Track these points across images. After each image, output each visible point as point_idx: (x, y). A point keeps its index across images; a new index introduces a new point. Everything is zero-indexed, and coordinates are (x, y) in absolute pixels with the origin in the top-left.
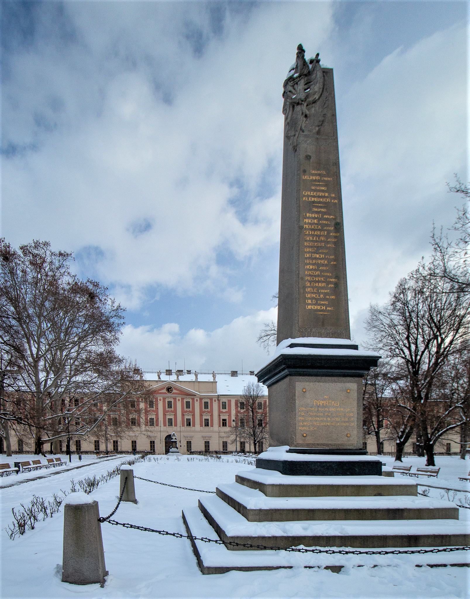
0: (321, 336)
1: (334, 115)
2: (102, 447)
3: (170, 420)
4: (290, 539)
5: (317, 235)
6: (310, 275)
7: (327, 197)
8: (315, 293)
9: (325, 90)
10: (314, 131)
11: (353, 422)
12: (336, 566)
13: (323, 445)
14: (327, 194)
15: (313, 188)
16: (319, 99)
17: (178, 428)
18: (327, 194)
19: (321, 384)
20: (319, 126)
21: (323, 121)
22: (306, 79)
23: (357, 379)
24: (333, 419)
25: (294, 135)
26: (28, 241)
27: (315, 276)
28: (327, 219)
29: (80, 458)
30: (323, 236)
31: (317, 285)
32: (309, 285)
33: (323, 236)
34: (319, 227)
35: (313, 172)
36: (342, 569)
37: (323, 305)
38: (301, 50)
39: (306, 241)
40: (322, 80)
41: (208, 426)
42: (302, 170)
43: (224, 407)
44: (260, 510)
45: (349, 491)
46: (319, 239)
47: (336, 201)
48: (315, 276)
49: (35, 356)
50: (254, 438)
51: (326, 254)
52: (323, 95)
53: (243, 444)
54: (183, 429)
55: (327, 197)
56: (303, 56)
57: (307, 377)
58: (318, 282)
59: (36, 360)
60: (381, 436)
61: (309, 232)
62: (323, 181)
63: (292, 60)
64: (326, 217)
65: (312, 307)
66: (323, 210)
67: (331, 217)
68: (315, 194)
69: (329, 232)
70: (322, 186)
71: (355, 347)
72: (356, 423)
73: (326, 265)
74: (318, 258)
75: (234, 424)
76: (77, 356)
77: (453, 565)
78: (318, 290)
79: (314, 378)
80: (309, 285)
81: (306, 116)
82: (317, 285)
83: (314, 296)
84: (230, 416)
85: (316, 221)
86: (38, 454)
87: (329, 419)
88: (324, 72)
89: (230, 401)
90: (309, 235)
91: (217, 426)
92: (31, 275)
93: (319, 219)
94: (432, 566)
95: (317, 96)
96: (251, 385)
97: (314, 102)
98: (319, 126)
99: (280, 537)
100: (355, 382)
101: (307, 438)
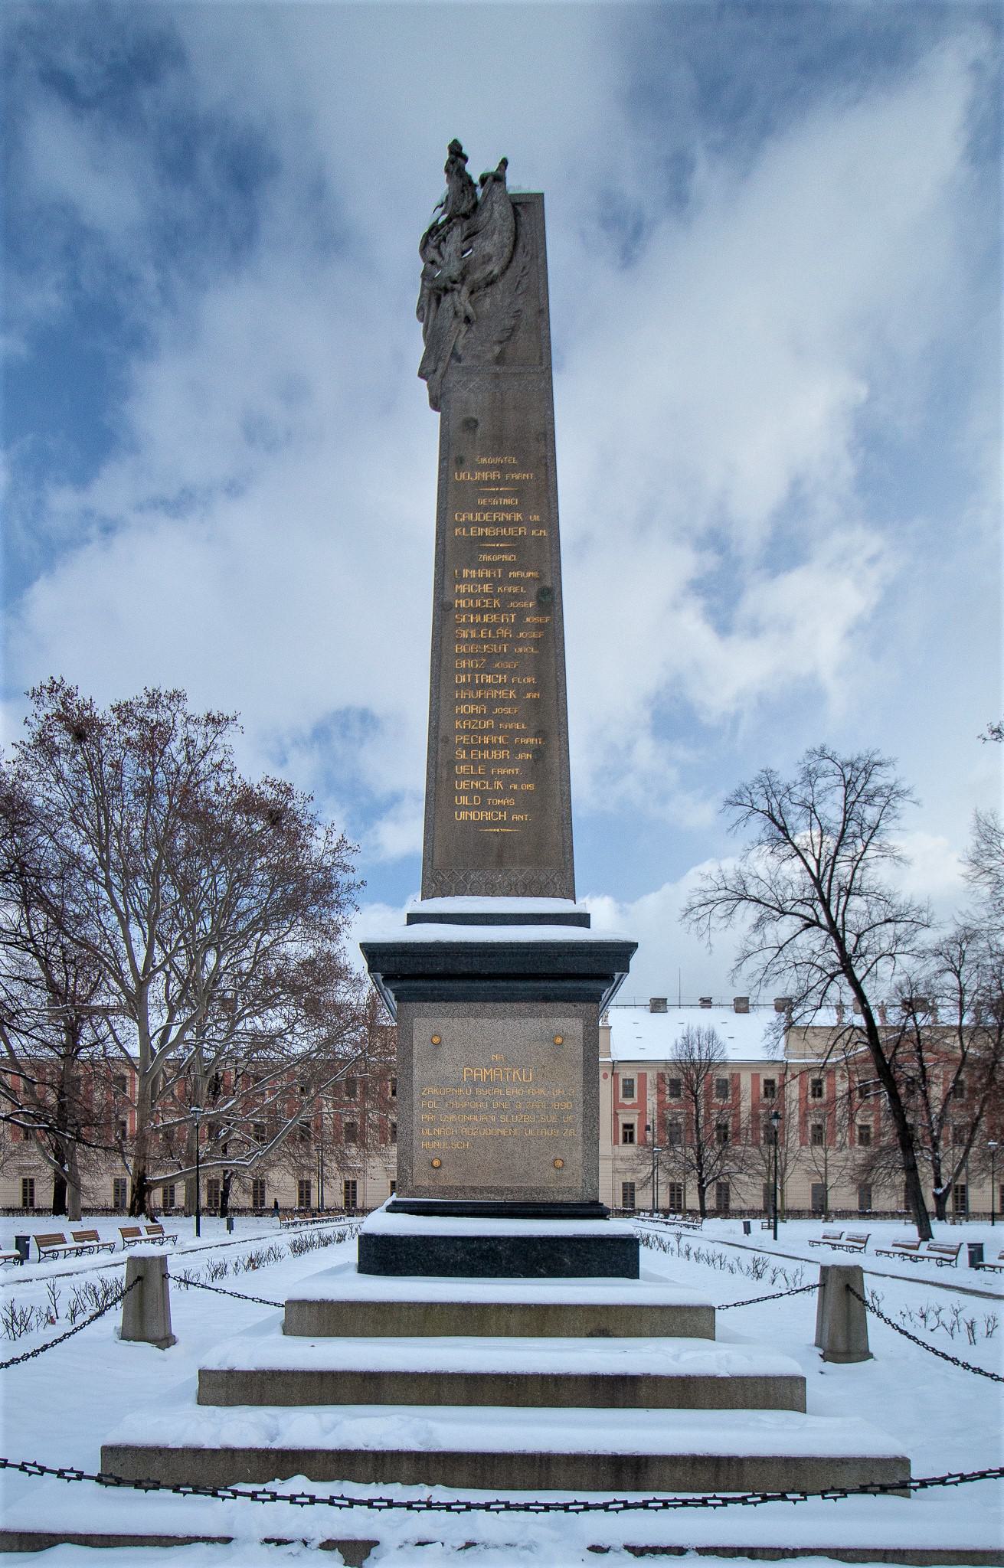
0: (491, 891)
1: (543, 312)
2: (692, 1201)
4: (272, 1457)
5: (488, 625)
6: (468, 731)
7: (519, 524)
8: (481, 777)
9: (520, 250)
10: (489, 356)
11: (571, 1126)
12: (355, 1542)
13: (490, 1190)
14: (518, 517)
15: (482, 502)
16: (503, 272)
18: (518, 517)
19: (484, 1021)
20: (501, 342)
21: (513, 329)
22: (465, 225)
23: (581, 1006)
24: (515, 1119)
25: (435, 371)
26: (132, 692)
27: (482, 732)
28: (517, 582)
29: (230, 1227)
31: (486, 755)
32: (463, 756)
35: (484, 460)
36: (374, 1551)
37: (502, 808)
38: (457, 153)
39: (459, 640)
40: (509, 224)
41: (632, 1141)
42: (453, 456)
43: (628, 1092)
44: (231, 1373)
45: (514, 1320)
46: (494, 633)
47: (543, 532)
48: (482, 732)
49: (141, 971)
50: (700, 1174)
52: (514, 264)
53: (676, 1192)
55: (519, 524)
57: (443, 1004)
58: (490, 747)
59: (144, 980)
61: (468, 618)
62: (507, 483)
63: (440, 187)
64: (516, 574)
65: (472, 815)
66: (506, 558)
67: (529, 574)
68: (486, 517)
69: (521, 613)
71: (583, 920)
72: (580, 1131)
73: (512, 703)
74: (490, 686)
76: (253, 969)
77: (704, 1551)
78: (488, 770)
79: (464, 1007)
80: (463, 756)
81: (468, 320)
82: (486, 755)
83: (478, 785)
84: (643, 1115)
86: (138, 1215)
87: (504, 1118)
88: (514, 205)
89: (643, 1077)
90: (468, 625)
91: (610, 1142)
92: (132, 770)
93: (495, 582)
94: (639, 1551)
95: (495, 268)
96: (694, 1033)
97: (491, 282)
98: (501, 342)
99: (243, 1450)
100: (577, 1016)
101: (443, 1172)
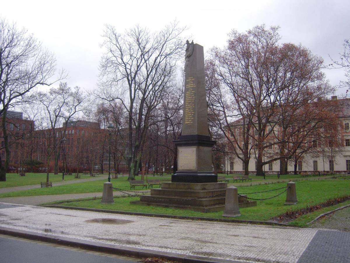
58: (189, 114)
85: (191, 99)
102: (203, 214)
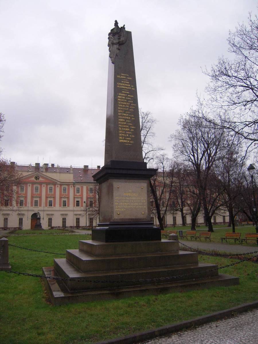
3: (36, 202)
5: (124, 105)
14: (129, 85)
15: (122, 82)
17: (41, 208)
18: (129, 85)
28: (129, 97)
30: (128, 105)
31: (125, 129)
32: (120, 129)
33: (128, 105)
34: (126, 100)
35: (123, 74)
38: (116, 23)
51: (129, 114)
54: (46, 208)
56: (118, 25)
58: (126, 128)
60: (184, 212)
64: (129, 96)
65: (123, 141)
66: (127, 92)
70: (127, 81)
75: (84, 205)
84: (82, 198)
85: (124, 98)
90: (120, 104)
102: (193, 320)
